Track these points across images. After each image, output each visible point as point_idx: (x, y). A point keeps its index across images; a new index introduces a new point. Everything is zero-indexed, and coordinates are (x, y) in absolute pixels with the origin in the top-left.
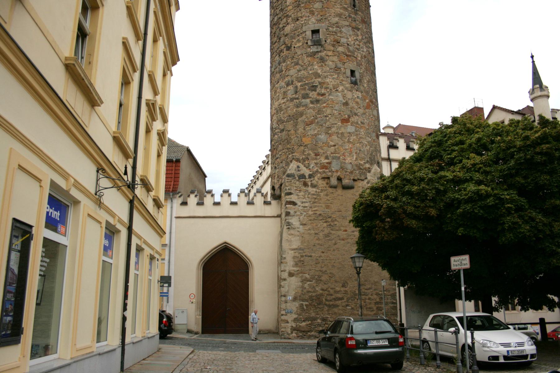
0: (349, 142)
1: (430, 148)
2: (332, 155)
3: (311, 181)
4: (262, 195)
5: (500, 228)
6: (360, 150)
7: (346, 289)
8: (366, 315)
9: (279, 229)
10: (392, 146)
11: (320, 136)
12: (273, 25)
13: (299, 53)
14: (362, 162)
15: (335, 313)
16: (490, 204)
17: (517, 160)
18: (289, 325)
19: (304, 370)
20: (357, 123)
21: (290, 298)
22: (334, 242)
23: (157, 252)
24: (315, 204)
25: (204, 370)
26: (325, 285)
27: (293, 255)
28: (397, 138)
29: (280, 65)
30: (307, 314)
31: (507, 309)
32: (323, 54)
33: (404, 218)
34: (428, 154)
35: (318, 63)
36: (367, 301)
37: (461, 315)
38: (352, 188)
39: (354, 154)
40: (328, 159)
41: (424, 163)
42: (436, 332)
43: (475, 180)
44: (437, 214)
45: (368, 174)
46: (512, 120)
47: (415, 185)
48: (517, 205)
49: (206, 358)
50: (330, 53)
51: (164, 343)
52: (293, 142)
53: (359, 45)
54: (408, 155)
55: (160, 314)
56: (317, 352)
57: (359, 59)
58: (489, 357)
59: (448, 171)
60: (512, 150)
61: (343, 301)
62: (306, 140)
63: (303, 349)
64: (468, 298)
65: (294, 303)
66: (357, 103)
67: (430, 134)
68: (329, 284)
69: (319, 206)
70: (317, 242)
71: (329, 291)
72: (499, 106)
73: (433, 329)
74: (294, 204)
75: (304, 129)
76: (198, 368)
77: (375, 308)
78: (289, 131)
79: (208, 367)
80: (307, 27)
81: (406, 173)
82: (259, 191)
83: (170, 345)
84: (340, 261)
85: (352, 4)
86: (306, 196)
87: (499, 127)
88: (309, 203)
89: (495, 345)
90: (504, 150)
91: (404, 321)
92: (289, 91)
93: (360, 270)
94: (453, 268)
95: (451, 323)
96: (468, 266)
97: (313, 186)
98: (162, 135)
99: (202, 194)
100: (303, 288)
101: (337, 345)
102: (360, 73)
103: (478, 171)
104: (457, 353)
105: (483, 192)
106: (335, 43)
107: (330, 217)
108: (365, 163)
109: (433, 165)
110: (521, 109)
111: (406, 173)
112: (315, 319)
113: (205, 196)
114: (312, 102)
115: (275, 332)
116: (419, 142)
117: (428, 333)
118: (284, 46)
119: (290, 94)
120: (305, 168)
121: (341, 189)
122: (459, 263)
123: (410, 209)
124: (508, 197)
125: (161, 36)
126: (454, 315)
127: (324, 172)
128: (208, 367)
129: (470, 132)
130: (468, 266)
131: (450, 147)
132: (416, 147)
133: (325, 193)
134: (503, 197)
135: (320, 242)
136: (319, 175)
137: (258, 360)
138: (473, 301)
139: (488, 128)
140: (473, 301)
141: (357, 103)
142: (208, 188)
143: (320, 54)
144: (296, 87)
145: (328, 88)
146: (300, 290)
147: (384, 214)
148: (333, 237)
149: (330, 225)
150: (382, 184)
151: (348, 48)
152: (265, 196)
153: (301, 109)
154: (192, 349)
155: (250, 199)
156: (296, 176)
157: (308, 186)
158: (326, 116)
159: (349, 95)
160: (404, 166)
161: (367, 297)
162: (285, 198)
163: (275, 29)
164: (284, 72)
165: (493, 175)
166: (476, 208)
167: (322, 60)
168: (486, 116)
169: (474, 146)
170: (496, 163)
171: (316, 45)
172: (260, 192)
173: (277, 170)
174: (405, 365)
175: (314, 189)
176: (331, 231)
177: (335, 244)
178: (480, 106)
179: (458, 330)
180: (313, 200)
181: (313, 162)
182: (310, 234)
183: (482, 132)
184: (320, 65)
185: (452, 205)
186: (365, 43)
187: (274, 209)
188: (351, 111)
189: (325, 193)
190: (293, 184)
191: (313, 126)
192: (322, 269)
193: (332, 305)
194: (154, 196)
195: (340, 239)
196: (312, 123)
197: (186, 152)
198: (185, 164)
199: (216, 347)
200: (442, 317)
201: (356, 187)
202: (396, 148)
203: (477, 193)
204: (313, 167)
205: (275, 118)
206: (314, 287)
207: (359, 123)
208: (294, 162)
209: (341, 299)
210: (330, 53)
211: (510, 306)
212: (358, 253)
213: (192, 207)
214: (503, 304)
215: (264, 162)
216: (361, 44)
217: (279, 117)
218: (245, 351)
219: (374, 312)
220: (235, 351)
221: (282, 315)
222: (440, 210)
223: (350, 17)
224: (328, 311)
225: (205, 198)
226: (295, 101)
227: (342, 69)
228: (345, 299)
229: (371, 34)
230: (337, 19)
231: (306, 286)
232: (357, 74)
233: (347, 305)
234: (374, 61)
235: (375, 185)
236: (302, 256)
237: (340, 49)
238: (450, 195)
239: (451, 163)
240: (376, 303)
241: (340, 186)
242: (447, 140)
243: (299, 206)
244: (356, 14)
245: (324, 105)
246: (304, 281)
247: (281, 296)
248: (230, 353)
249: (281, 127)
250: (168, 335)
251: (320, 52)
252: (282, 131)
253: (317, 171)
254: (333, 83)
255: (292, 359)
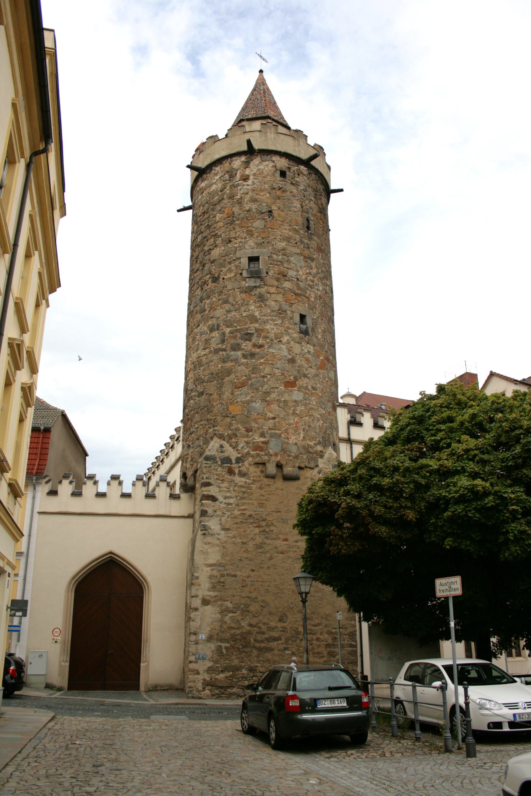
0: (294, 413)
1: (407, 426)
2: (270, 432)
3: (240, 467)
4: (168, 484)
5: (502, 539)
6: (309, 426)
7: (285, 625)
8: (313, 663)
9: (190, 535)
10: (354, 422)
11: (254, 404)
12: (195, 246)
13: (229, 287)
14: (312, 443)
15: (268, 661)
16: (489, 505)
17: (525, 445)
18: (200, 677)
19: (223, 746)
20: (307, 388)
21: (203, 636)
22: (268, 555)
23: (9, 563)
24: (244, 501)
25: (71, 746)
26: (255, 619)
27: (209, 574)
28: (362, 410)
29: (202, 302)
30: (227, 662)
31: (510, 655)
32: (263, 290)
33: (370, 523)
34: (405, 434)
35: (255, 302)
36: (314, 642)
37: (450, 662)
38: (296, 478)
39: (301, 431)
40: (265, 437)
41: (398, 447)
42: (414, 687)
43: (468, 472)
44: (416, 518)
45: (320, 460)
46: (516, 391)
47: (386, 476)
48: (525, 507)
49: (74, 728)
50: (273, 290)
51: (9, 705)
52: (215, 410)
53: (313, 281)
54: (377, 435)
55: (6, 659)
56: (242, 718)
57: (313, 299)
58: (489, 724)
59: (431, 458)
60: (517, 432)
61: (280, 642)
62: (235, 410)
63: (219, 713)
64: (458, 639)
65: (209, 645)
66: (307, 360)
67: (408, 407)
68: (261, 618)
69: (249, 504)
70: (245, 555)
71: (260, 628)
72: (498, 372)
73: (410, 683)
74: (214, 499)
75: (232, 394)
76: (62, 744)
77: (325, 653)
78: (211, 395)
79: (78, 742)
80: (242, 252)
81: (374, 460)
82: (163, 479)
83: (18, 708)
84: (277, 583)
85: (306, 226)
86: (232, 489)
87: (500, 401)
88: (235, 499)
89: (497, 707)
90: (507, 432)
91: (367, 672)
92: (213, 339)
93: (306, 597)
94: (439, 594)
95: (436, 674)
96: (459, 592)
97: (242, 474)
98: (28, 391)
99: (80, 479)
100: (222, 621)
101: (273, 707)
102: (313, 319)
103: (472, 460)
104: (445, 718)
105: (480, 488)
106: (280, 276)
107: (264, 520)
108: (316, 445)
109: (411, 450)
110: (526, 377)
111: (374, 460)
112: (239, 669)
113: (85, 483)
114: (245, 356)
115: (179, 689)
116: (392, 418)
117: (402, 689)
118: (209, 276)
119: (214, 344)
120: (230, 449)
121: (281, 480)
122: (447, 587)
123: (378, 510)
124: (513, 496)
125: (36, 250)
126: (439, 663)
127: (258, 455)
128: (78, 742)
129: (461, 405)
130: (459, 592)
131: (435, 426)
132: (387, 424)
133: (259, 484)
134: (506, 495)
135: (249, 555)
136: (250, 459)
137: (154, 730)
138: (463, 642)
139: (485, 402)
140: (463, 642)
141: (307, 360)
142: (89, 472)
143: (258, 290)
144: (224, 334)
145: (268, 337)
146: (217, 625)
147: (343, 518)
148: (267, 548)
149: (264, 531)
150: (340, 474)
151: (297, 285)
152: (171, 486)
153: (229, 364)
154: (53, 714)
155: (150, 489)
156: (218, 459)
157: (235, 474)
158: (263, 377)
159: (297, 349)
160: (371, 449)
161: (315, 637)
162: (200, 491)
163: (197, 252)
164: (207, 312)
165: (492, 466)
166: (470, 510)
167: (261, 298)
168: (480, 386)
169: (467, 424)
170: (496, 449)
171: (253, 277)
172: (165, 480)
173: (191, 450)
174: (370, 737)
175: (243, 479)
176: (266, 540)
177: (271, 558)
178: (473, 371)
179: (446, 684)
180: (241, 495)
181: (243, 440)
182: (234, 543)
183: (478, 406)
184: (258, 305)
185: (438, 505)
186: (321, 279)
187: (183, 506)
188: (298, 371)
189: (259, 484)
190: (213, 471)
191: (245, 389)
192: (250, 595)
193: (264, 648)
194: (10, 479)
195: (277, 552)
196: (243, 385)
197: (60, 417)
198: (57, 436)
199: (89, 710)
200: (422, 667)
201: (302, 478)
202: (360, 424)
203: (472, 490)
204: (242, 447)
205: (191, 375)
206: (238, 621)
207: (310, 387)
208: (216, 439)
209: (278, 639)
210: (273, 290)
211: (514, 651)
212: (304, 571)
213: (65, 499)
214: (504, 649)
215: (172, 437)
216: (315, 279)
217: (197, 375)
218: (133, 717)
219: (325, 659)
220: (118, 717)
221: (191, 662)
222: (420, 512)
223: (302, 242)
224: (258, 656)
225: (84, 487)
226: (221, 353)
227: (289, 312)
228: (283, 639)
229: (330, 267)
230: (283, 244)
231: (227, 619)
232: (308, 320)
233: (286, 649)
234: (332, 303)
235: (331, 476)
236: (222, 576)
237: (287, 285)
238: (434, 491)
239: (436, 447)
240: (328, 646)
241: (280, 475)
242: (430, 416)
243: (221, 502)
244: (310, 239)
245: (262, 361)
246: (224, 611)
247: (190, 633)
248: (111, 720)
249: (200, 389)
250: (16, 693)
251: (259, 287)
252: (201, 394)
253: (248, 453)
254: (275, 330)
255: (204, 729)
